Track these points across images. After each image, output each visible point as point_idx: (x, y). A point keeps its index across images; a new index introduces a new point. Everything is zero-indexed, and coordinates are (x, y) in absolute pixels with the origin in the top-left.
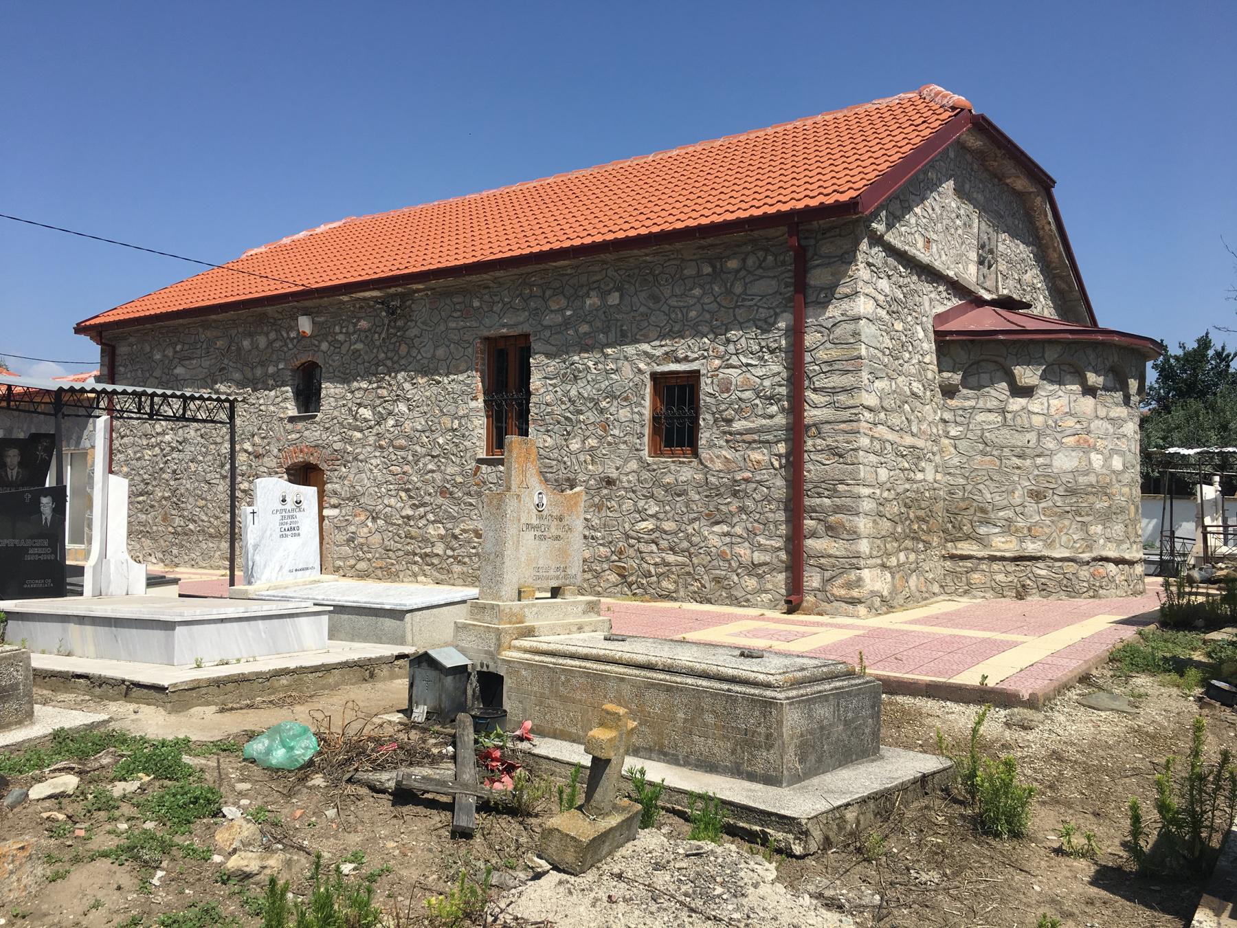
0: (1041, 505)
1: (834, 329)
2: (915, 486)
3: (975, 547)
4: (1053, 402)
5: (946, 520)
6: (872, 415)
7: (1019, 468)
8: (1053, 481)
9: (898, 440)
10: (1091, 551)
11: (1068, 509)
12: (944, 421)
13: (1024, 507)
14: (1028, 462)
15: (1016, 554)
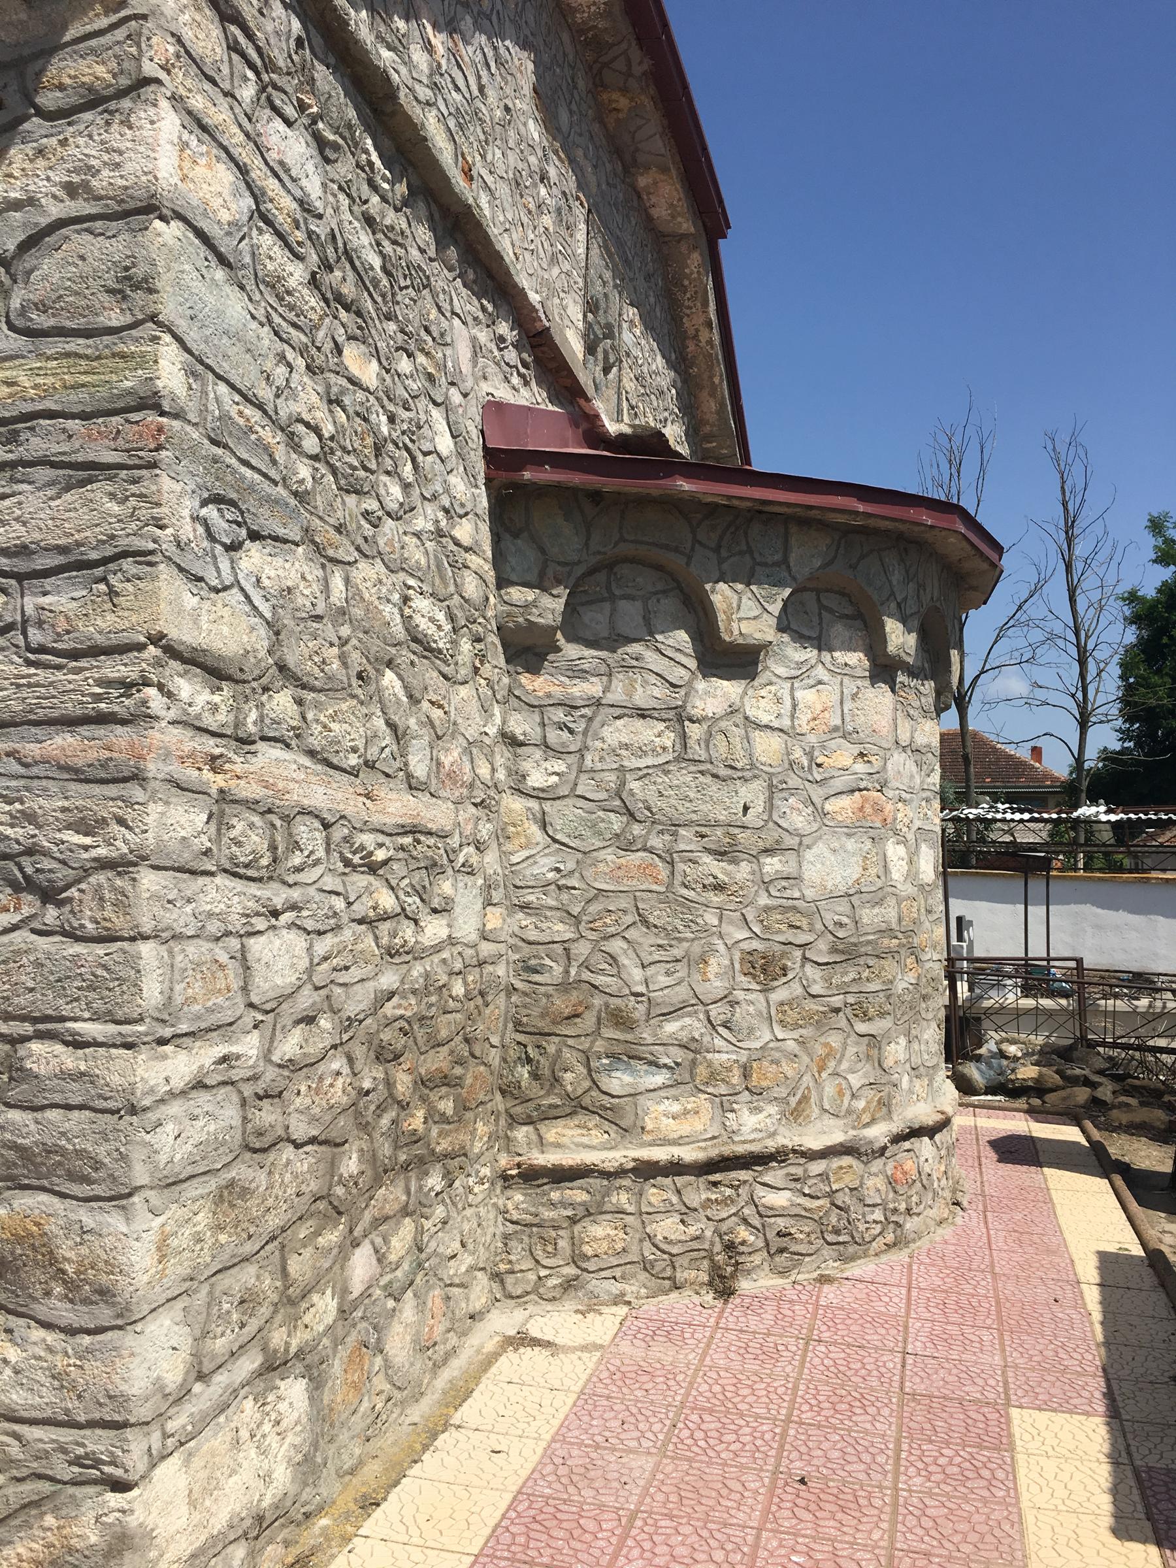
0: (775, 997)
1: (29, 261)
2: (417, 970)
3: (597, 1137)
4: (806, 696)
5: (513, 1054)
6: (224, 696)
7: (719, 887)
8: (804, 923)
9: (354, 807)
10: (889, 1116)
11: (837, 1001)
12: (511, 741)
13: (734, 1004)
14: (743, 871)
15: (713, 1153)
